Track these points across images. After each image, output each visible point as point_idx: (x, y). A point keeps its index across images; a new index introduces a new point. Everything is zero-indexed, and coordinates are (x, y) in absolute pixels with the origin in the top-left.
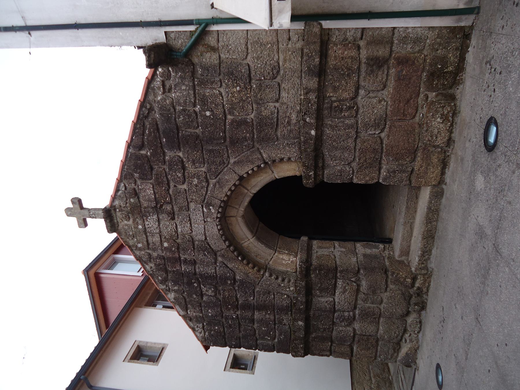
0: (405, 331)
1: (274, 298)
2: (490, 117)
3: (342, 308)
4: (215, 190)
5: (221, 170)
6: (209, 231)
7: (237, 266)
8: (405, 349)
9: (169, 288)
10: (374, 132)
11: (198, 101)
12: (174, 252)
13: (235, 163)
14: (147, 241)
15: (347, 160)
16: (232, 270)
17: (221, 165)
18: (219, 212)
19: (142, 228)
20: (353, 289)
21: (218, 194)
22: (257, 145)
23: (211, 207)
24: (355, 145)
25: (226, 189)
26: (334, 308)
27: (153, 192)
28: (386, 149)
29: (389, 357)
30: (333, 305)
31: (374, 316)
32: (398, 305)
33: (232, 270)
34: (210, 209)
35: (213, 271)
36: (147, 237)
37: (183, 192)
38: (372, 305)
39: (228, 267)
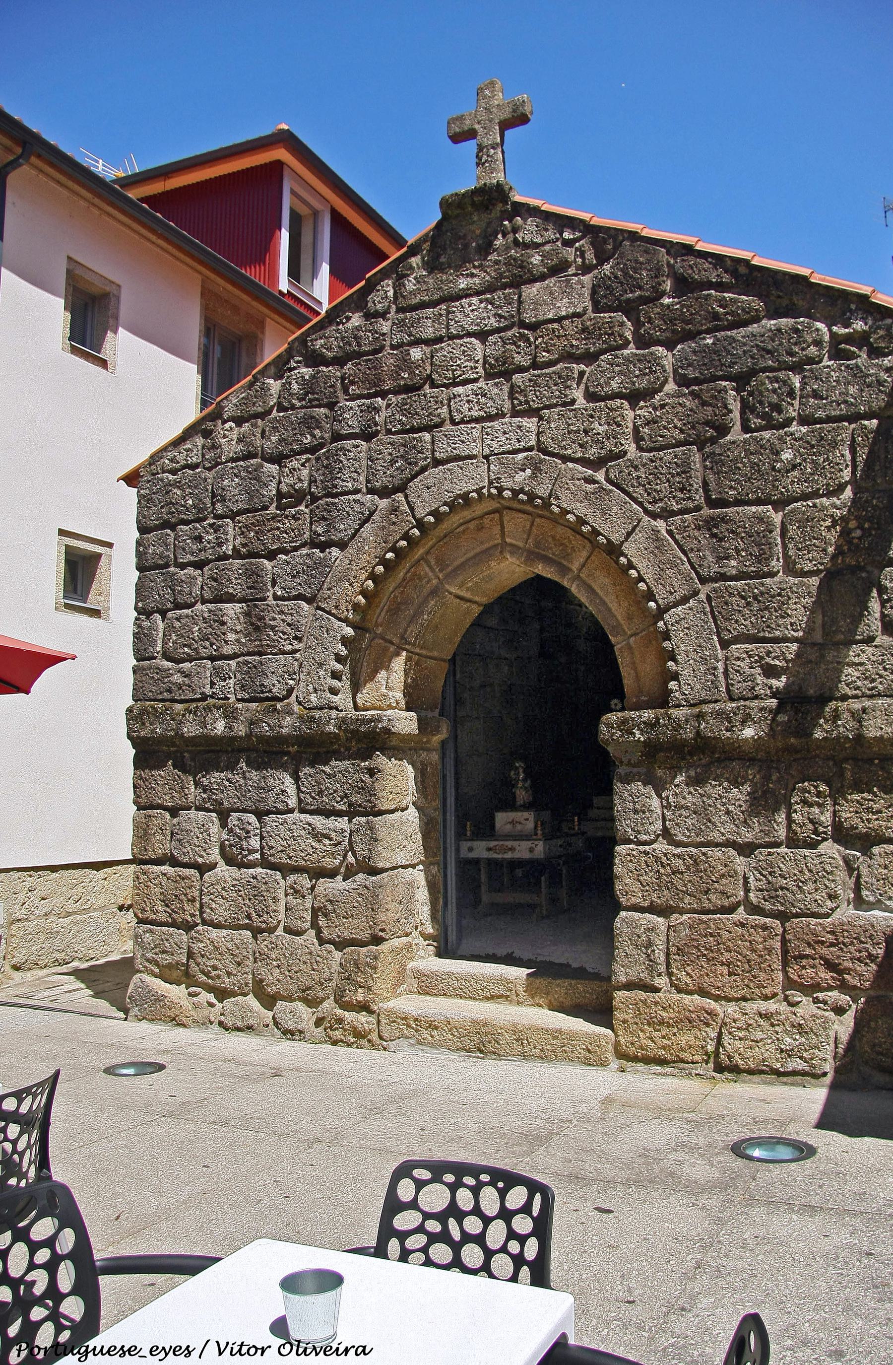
0: (222, 994)
1: (284, 653)
2: (815, 1145)
3: (268, 832)
4: (579, 479)
5: (635, 495)
6: (461, 468)
7: (367, 548)
8: (176, 993)
9: (295, 368)
10: (753, 888)
11: (820, 428)
12: (396, 376)
13: (656, 532)
14: (423, 305)
15: (677, 824)
16: (354, 535)
17: (649, 494)
18: (515, 493)
19: (460, 290)
20: (324, 857)
21: (568, 489)
22: (704, 590)
23: (528, 471)
24: (717, 845)
25: (581, 509)
26: (268, 813)
27: (564, 313)
28: (709, 920)
29: (149, 955)
30: (276, 807)
31: (254, 914)
32: (289, 971)
33: (354, 535)
34: (524, 470)
35: (350, 485)
36: (434, 304)
37: (566, 396)
38: (282, 909)
39: (361, 526)
